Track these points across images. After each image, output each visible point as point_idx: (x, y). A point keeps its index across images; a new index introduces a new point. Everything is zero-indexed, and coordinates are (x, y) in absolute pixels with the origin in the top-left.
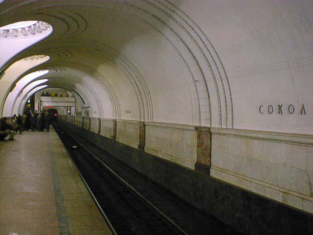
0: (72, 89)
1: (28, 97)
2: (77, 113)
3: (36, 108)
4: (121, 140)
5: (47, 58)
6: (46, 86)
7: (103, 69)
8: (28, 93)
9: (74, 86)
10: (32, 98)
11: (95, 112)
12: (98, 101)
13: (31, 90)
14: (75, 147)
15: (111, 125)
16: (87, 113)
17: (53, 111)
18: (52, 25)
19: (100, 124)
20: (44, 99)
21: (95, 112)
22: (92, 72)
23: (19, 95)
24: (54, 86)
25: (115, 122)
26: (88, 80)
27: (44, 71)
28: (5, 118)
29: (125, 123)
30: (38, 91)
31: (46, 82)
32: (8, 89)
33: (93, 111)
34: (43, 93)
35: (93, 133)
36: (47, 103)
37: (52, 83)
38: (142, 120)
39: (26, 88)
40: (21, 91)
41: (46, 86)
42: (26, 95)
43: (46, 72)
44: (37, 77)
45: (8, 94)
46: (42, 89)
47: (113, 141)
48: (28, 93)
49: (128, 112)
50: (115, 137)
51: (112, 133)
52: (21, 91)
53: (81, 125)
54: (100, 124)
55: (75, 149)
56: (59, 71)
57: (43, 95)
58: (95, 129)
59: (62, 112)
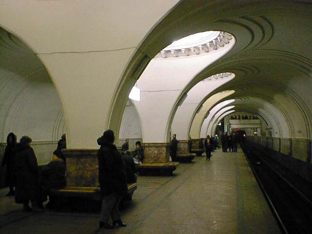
0: (257, 113)
1: (218, 121)
2: (262, 133)
3: (226, 130)
4: (295, 156)
5: (233, 92)
6: (234, 111)
7: (277, 98)
8: (215, 114)
9: (258, 111)
10: (222, 121)
11: (277, 133)
12: (278, 124)
13: (222, 114)
14: (259, 163)
15: (288, 143)
16: (270, 133)
17: (241, 132)
18: (234, 36)
19: (280, 143)
20: (232, 121)
21: (277, 133)
22: (270, 100)
23: (211, 120)
24: (241, 112)
25: (290, 140)
26: (268, 105)
27: (230, 91)
28: (202, 139)
29: (298, 141)
30: (226, 116)
31: (233, 102)
32: (194, 111)
33: (275, 132)
34: (232, 116)
35: (276, 151)
36: (235, 125)
37: (238, 108)
38: (309, 139)
39: (213, 108)
40: (214, 116)
41: (234, 111)
42: (217, 120)
43: (233, 100)
44: (221, 99)
45: (195, 114)
46: (230, 114)
47: (288, 157)
48: (215, 114)
49: (300, 132)
50: (291, 154)
51: (289, 151)
52: (214, 116)
53: (304, 159)
54: (280, 143)
55: (258, 165)
56: (243, 99)
57: (232, 118)
58: (276, 148)
59: (250, 133)
